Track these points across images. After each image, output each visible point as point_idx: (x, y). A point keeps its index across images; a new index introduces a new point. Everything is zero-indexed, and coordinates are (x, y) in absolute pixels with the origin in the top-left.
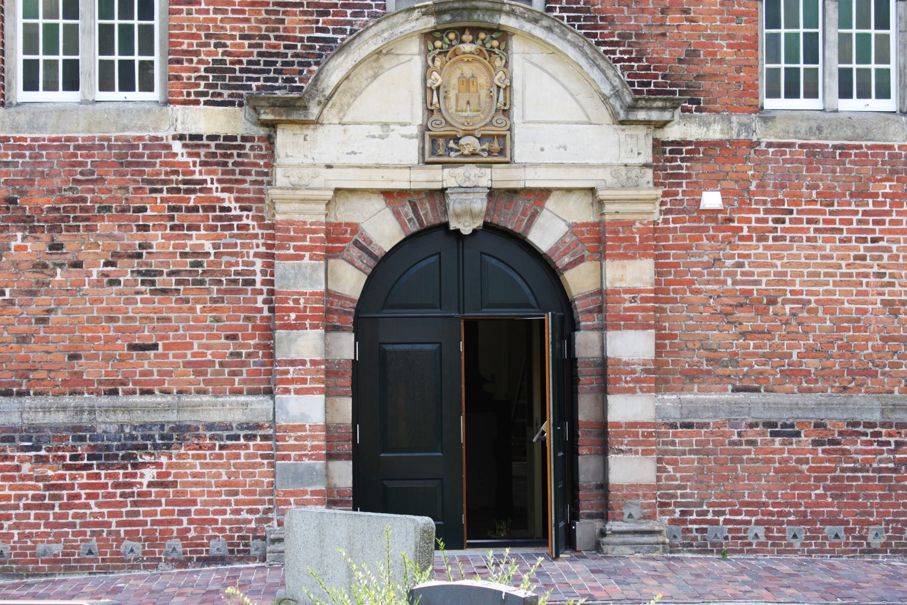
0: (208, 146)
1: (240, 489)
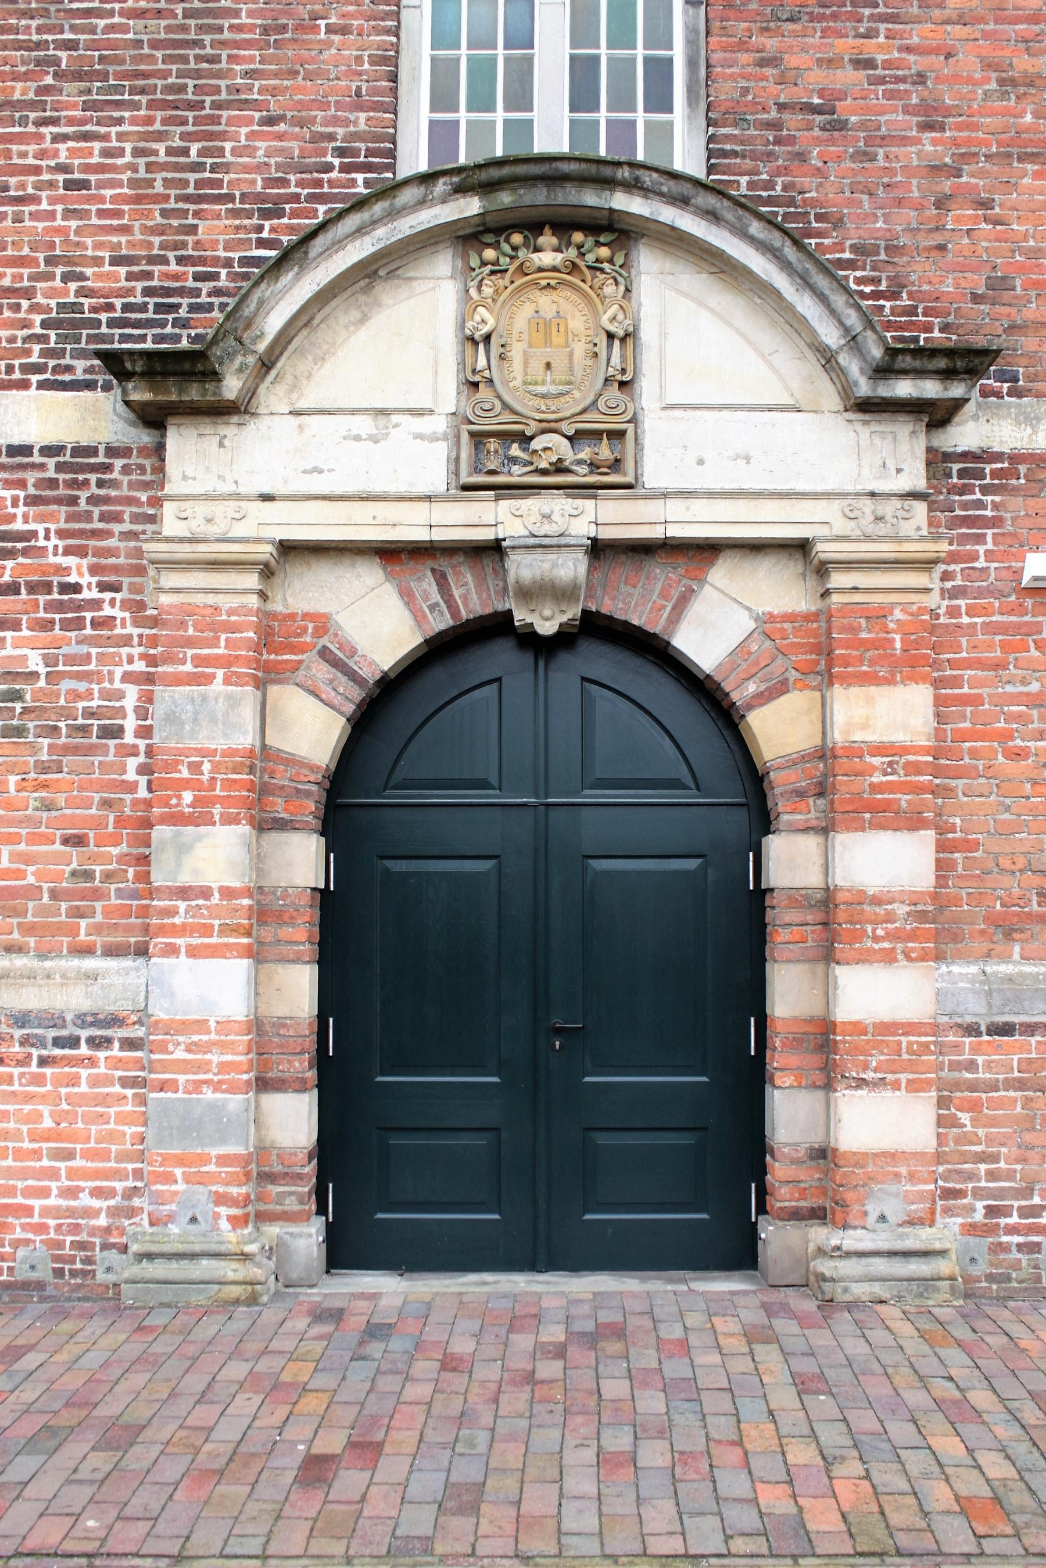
0: (42, 467)
1: (79, 1146)
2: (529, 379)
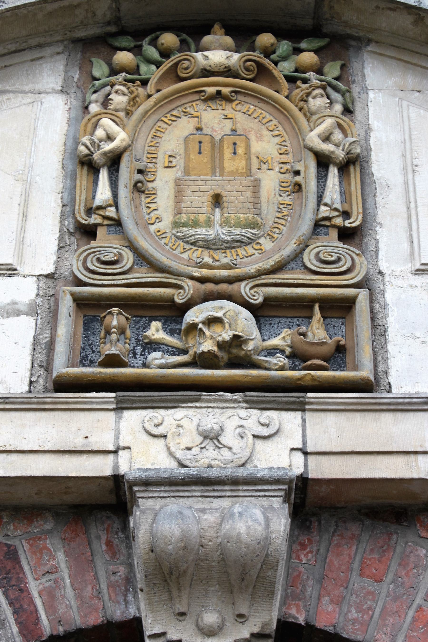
2: (184, 217)
